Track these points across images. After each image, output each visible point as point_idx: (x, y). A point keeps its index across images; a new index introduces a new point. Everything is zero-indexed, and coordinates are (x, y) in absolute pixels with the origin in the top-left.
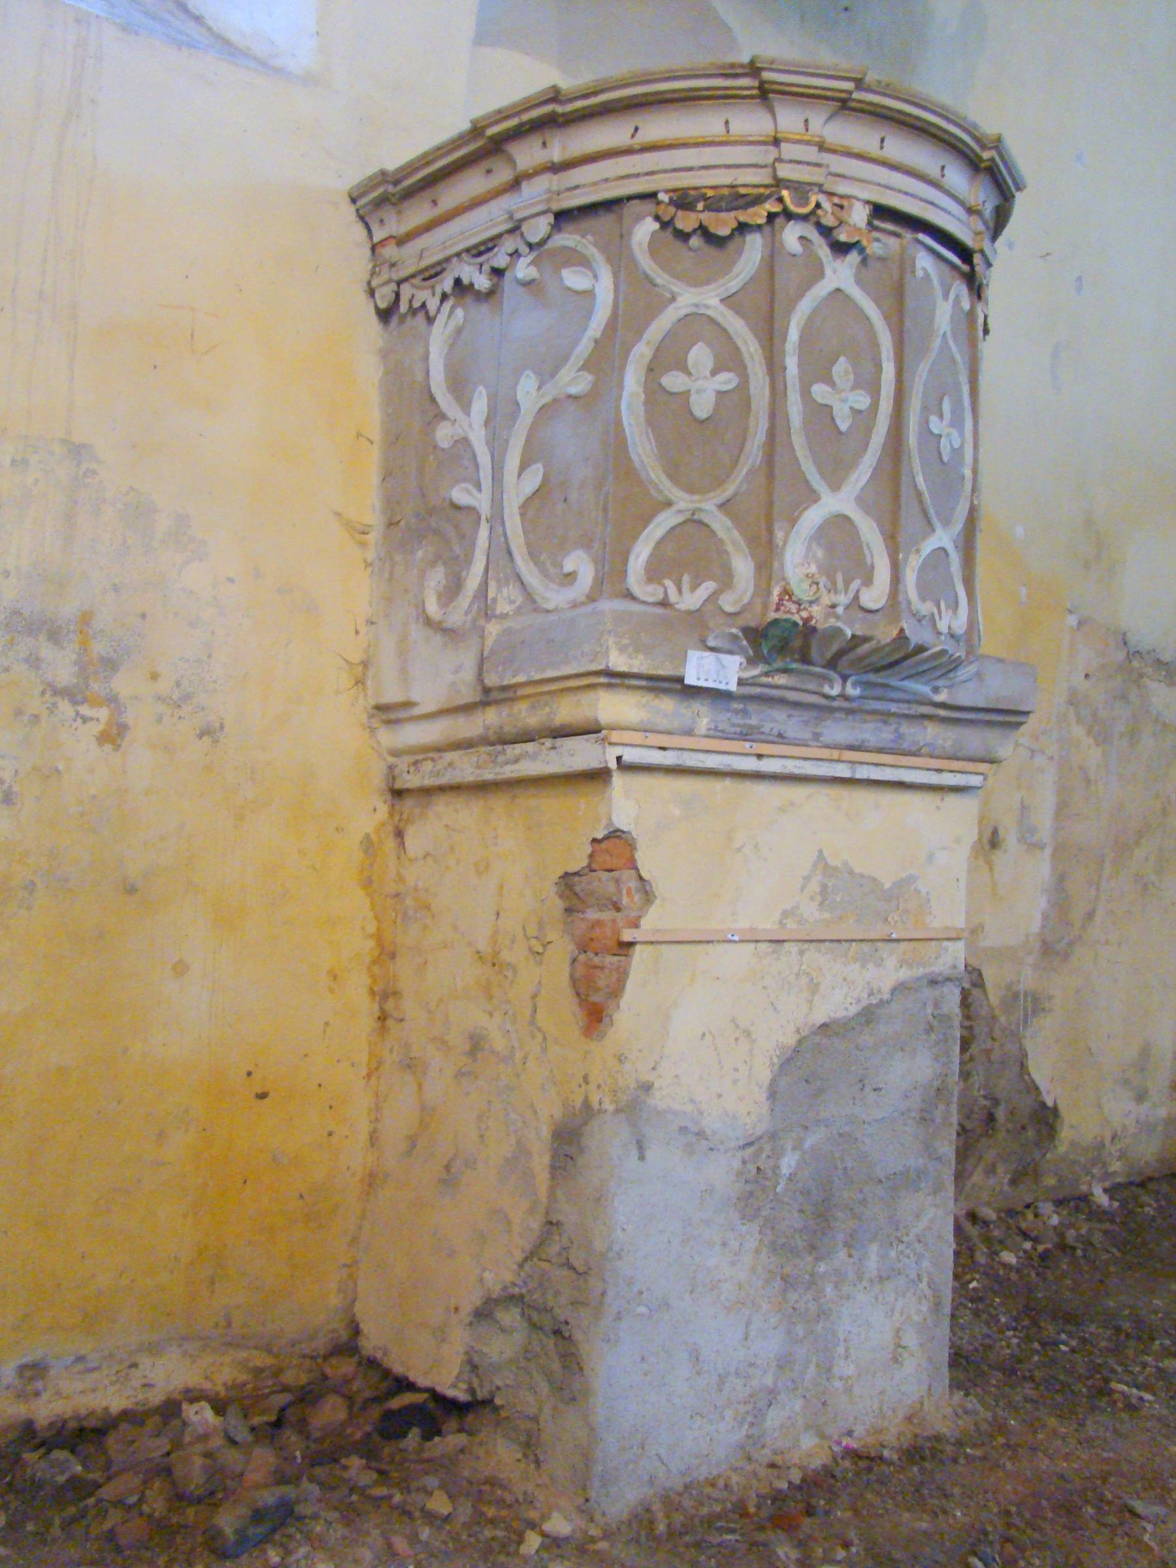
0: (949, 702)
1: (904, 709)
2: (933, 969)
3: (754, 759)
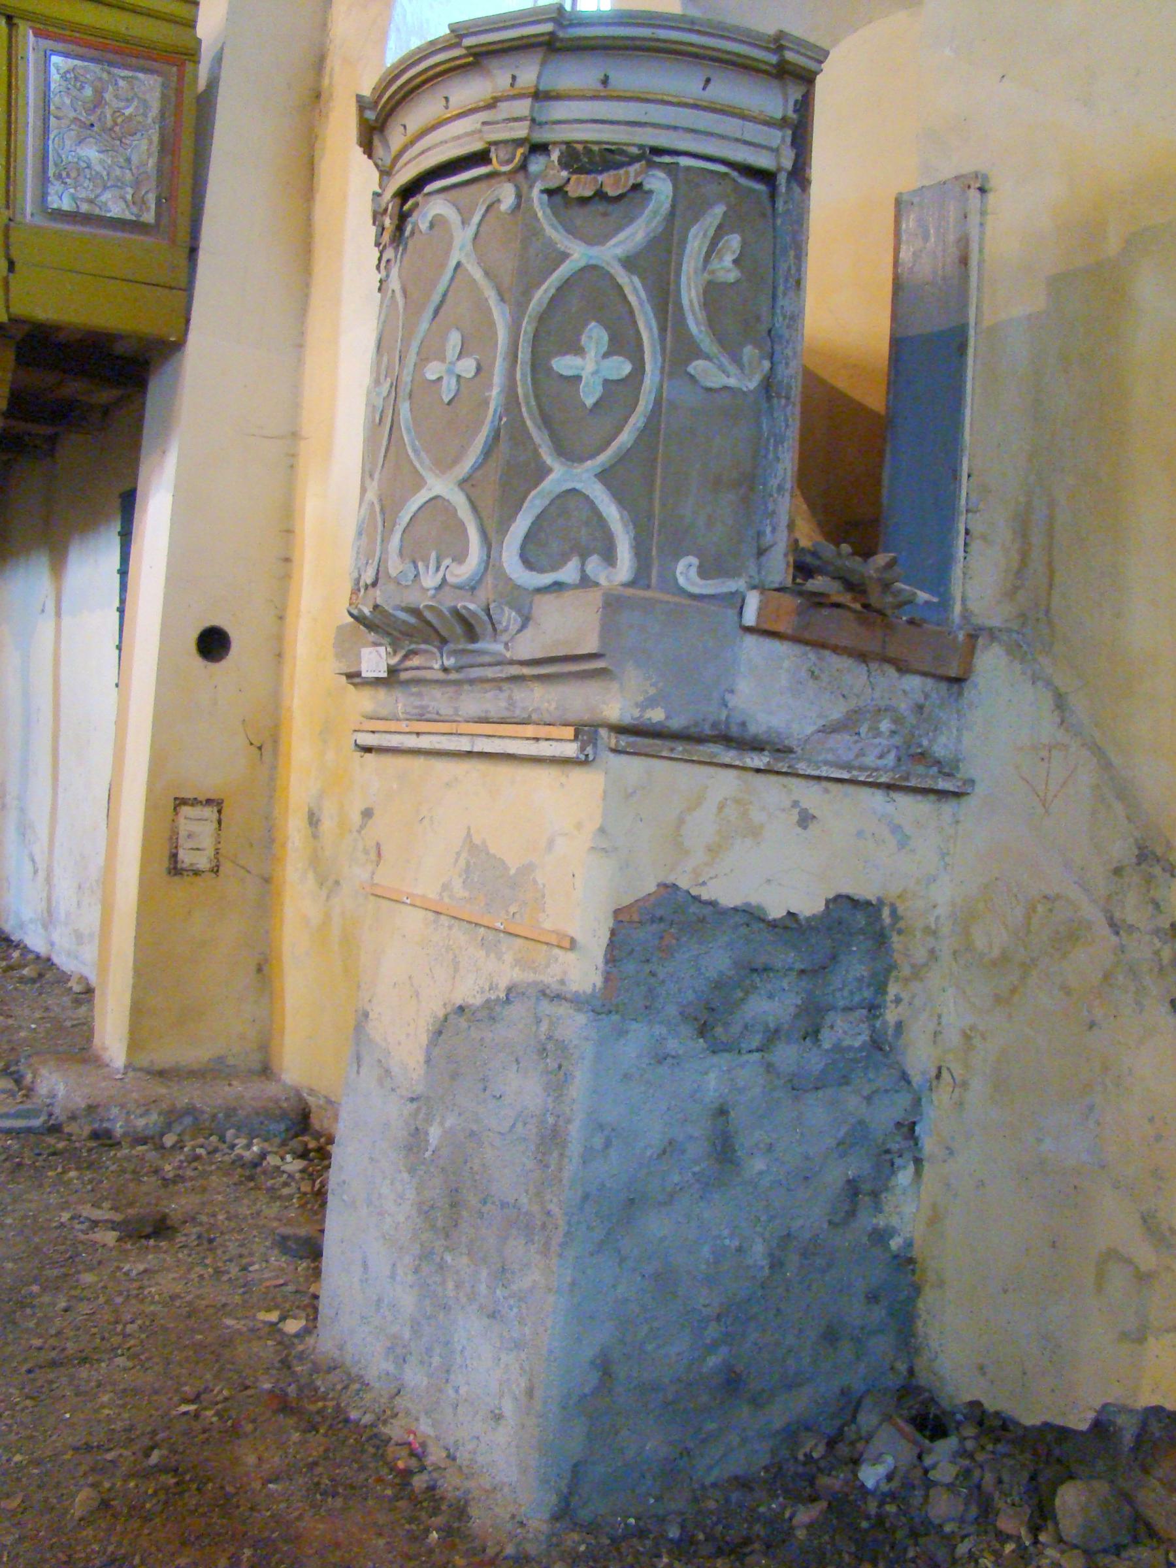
3: (414, 736)
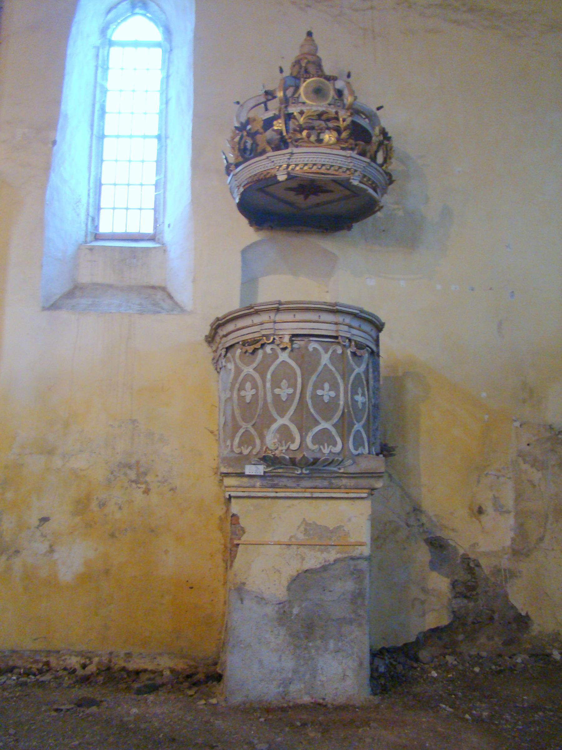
1: (329, 475)
2: (352, 555)
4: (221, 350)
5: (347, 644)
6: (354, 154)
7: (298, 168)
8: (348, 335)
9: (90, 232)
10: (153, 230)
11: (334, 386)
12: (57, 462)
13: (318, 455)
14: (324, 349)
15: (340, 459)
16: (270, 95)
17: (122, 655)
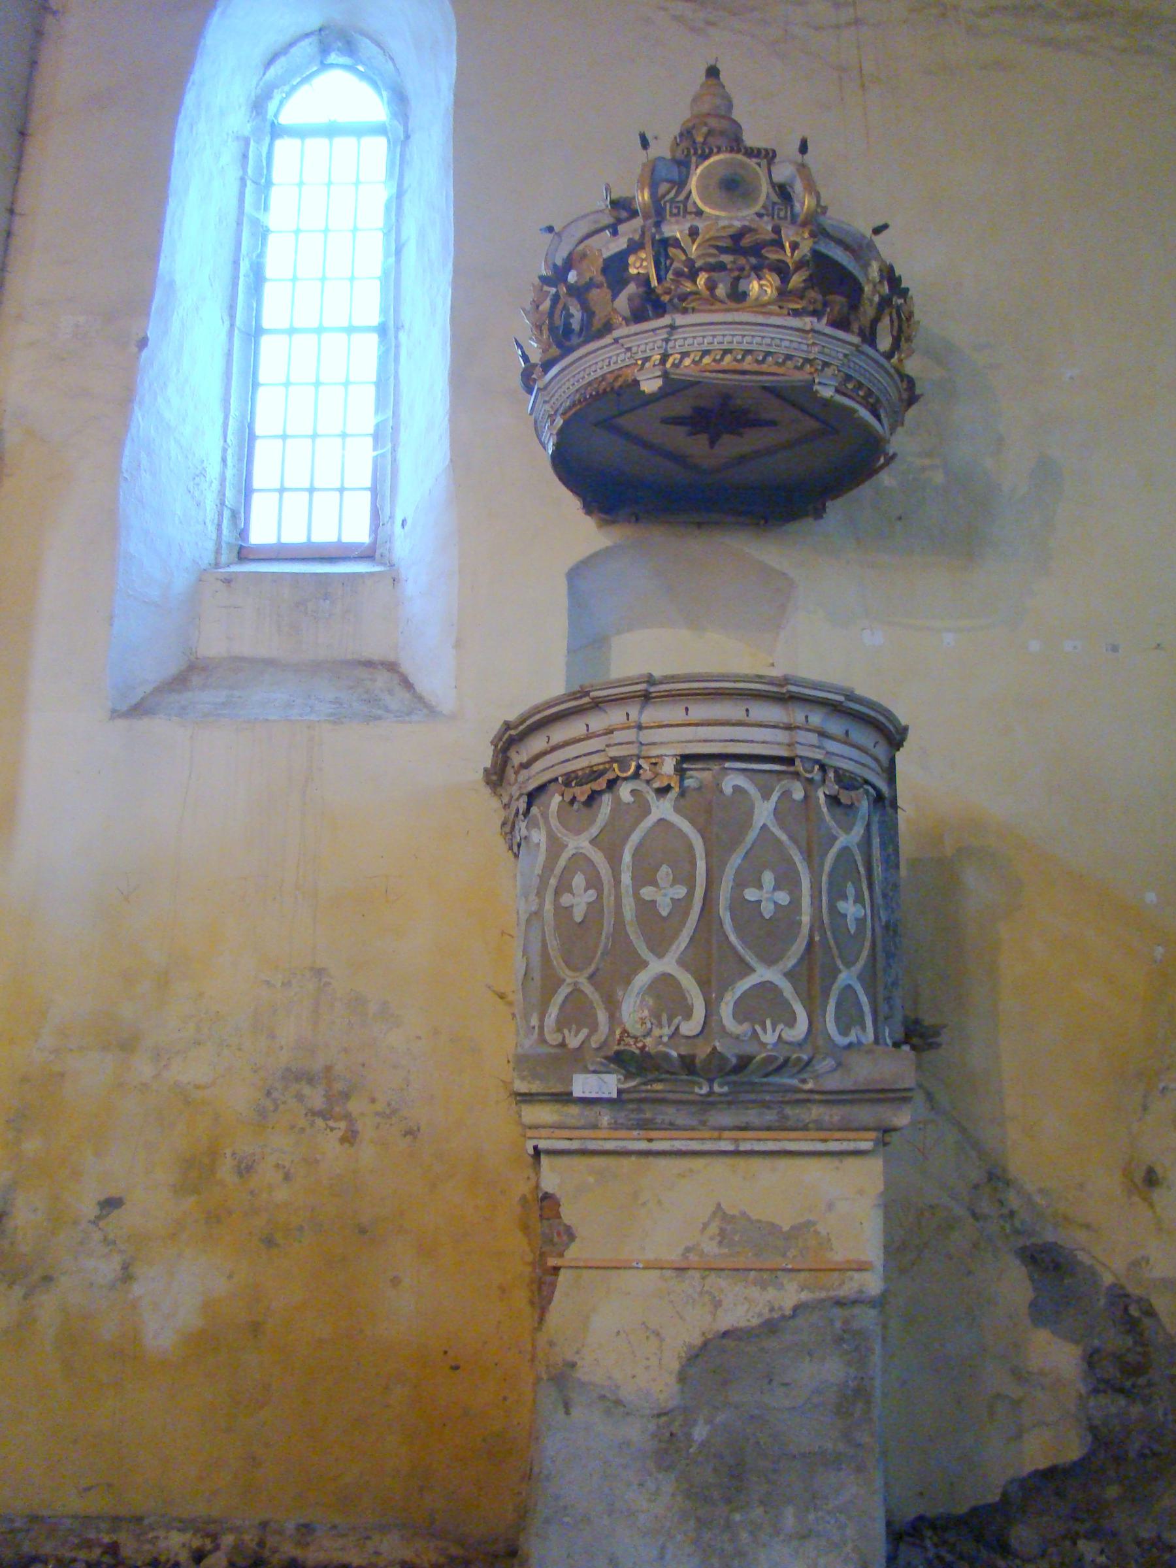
0: (817, 1088)
1: (779, 1097)
4: (518, 799)
5: (828, 1518)
6: (822, 325)
7: (687, 362)
8: (818, 754)
9: (228, 544)
10: (370, 536)
11: (787, 880)
12: (143, 1068)
13: (749, 1049)
14: (760, 788)
15: (805, 1057)
16: (622, 208)
17: (290, 1526)
